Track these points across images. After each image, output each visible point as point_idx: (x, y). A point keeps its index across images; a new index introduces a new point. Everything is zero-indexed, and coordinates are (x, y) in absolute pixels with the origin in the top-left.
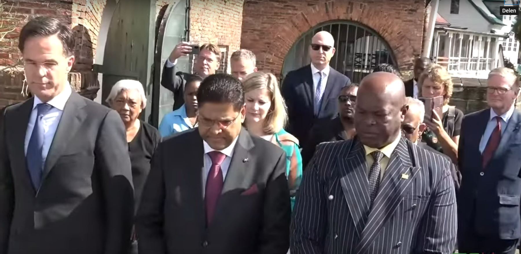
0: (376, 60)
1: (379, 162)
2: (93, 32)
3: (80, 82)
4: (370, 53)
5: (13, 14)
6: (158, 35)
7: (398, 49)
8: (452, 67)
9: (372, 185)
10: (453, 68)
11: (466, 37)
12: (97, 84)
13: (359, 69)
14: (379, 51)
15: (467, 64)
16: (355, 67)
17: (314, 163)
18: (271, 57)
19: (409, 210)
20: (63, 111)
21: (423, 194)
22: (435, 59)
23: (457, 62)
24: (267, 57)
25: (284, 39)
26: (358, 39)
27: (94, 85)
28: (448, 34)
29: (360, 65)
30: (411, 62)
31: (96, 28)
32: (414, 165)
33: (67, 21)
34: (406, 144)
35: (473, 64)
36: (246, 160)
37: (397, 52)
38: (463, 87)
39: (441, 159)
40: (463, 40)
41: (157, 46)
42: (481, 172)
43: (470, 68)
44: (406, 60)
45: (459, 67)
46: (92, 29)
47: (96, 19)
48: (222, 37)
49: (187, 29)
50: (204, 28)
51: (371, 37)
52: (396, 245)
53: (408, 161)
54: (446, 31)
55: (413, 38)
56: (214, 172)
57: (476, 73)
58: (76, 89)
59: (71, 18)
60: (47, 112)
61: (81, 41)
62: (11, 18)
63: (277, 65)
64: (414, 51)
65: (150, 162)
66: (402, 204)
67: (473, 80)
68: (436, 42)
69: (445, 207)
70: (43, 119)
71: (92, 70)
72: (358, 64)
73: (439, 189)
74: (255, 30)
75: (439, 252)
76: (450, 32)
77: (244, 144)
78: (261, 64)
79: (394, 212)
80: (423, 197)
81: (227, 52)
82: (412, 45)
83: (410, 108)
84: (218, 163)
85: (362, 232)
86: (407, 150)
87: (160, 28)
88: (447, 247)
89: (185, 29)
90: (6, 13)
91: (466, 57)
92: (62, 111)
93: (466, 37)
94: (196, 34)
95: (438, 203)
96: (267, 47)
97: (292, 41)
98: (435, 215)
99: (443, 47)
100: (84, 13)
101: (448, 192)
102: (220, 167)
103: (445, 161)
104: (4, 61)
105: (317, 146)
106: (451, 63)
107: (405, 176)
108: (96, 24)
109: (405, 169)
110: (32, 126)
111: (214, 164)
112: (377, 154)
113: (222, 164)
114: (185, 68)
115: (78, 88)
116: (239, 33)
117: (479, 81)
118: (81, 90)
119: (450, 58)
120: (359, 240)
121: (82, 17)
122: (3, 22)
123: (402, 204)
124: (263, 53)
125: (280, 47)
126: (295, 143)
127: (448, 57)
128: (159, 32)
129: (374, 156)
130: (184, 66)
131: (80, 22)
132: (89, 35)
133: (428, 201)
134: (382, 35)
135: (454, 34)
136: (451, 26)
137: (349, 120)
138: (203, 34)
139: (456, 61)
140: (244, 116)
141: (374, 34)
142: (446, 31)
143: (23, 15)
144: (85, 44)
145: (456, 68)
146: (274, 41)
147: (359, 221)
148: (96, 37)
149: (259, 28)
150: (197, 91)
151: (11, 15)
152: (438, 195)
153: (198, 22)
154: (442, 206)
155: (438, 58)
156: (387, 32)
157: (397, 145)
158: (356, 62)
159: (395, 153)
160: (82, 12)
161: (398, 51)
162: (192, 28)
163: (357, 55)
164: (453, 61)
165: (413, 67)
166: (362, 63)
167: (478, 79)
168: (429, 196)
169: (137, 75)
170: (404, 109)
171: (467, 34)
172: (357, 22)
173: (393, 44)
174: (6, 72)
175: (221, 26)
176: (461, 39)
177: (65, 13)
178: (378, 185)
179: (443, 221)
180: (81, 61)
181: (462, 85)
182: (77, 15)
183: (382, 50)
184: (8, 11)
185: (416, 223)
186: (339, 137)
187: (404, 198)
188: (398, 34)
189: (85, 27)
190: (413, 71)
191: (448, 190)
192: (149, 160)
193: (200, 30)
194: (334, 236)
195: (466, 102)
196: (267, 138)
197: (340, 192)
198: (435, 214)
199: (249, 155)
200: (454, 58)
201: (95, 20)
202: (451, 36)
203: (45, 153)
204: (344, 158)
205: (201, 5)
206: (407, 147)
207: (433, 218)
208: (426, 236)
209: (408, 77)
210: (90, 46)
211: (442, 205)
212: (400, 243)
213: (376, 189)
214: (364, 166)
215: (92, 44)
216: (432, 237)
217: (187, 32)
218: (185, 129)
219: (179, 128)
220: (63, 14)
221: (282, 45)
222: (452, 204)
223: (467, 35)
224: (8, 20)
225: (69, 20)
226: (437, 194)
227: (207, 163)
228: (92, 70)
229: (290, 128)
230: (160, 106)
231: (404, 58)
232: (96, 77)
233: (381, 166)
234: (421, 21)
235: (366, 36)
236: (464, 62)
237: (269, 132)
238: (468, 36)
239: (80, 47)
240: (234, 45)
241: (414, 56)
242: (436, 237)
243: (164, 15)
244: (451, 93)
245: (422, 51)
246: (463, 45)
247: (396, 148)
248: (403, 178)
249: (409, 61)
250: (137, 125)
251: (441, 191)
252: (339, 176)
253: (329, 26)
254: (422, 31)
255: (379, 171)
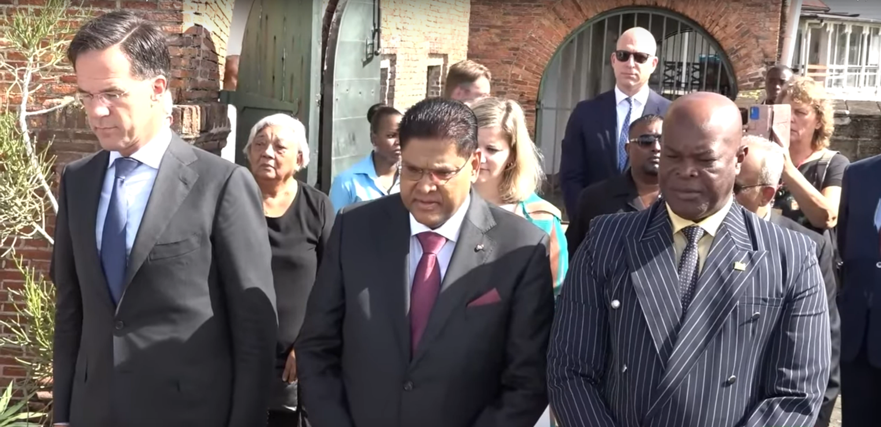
0: (700, 74)
1: (697, 243)
2: (219, 37)
3: (199, 120)
4: (689, 61)
5: (87, 9)
6: (329, 39)
7: (738, 54)
8: (833, 82)
9: (686, 283)
10: (835, 84)
11: (857, 31)
12: (227, 124)
13: (671, 89)
14: (704, 58)
15: (859, 76)
16: (664, 86)
17: (587, 247)
18: (520, 72)
19: (749, 322)
20: (158, 170)
21: (770, 295)
22: (803, 70)
23: (841, 74)
24: (513, 72)
25: (540, 41)
26: (669, 39)
27: (223, 125)
28: (826, 25)
29: (673, 81)
30: (761, 75)
31: (224, 28)
32: (755, 248)
33: (175, 19)
34: (741, 213)
35: (870, 76)
36: (479, 247)
37: (736, 58)
38: (850, 116)
39: (800, 238)
40: (852, 35)
41: (326, 57)
42: (878, 262)
43: (865, 83)
44: (751, 71)
45: (844, 83)
46: (218, 32)
47: (224, 15)
48: (436, 40)
49: (376, 28)
50: (405, 26)
51: (691, 33)
52: (726, 380)
53: (745, 241)
54: (822, 20)
55: (762, 34)
56: (426, 267)
57: (876, 92)
58: (192, 132)
59: (182, 14)
60: (131, 172)
61: (200, 53)
62: (83, 16)
63: (530, 84)
64: (766, 56)
65: (317, 250)
66: (735, 311)
67: (869, 103)
68: (805, 40)
69: (809, 317)
70: (124, 185)
71: (219, 100)
72: (669, 81)
73: (798, 287)
74: (491, 27)
75: (802, 392)
76: (828, 23)
77: (477, 221)
78: (504, 85)
79: (722, 325)
80: (771, 301)
81: (445, 65)
82: (762, 46)
83: (749, 151)
84: (433, 252)
85: (668, 359)
86: (744, 224)
87: (331, 28)
88: (814, 384)
89: (373, 29)
90: (76, 8)
91: (857, 64)
92: (156, 169)
93: (857, 31)
94: (392, 36)
95: (797, 310)
96: (512, 55)
97: (555, 44)
98: (793, 330)
99: (816, 48)
100: (204, 5)
101: (814, 292)
102: (436, 259)
103: (808, 242)
104: (73, 88)
105: (592, 220)
106: (832, 75)
107: (740, 266)
108: (224, 23)
109: (739, 253)
110: (107, 196)
111: (426, 254)
112: (693, 231)
113: (441, 253)
114: (373, 95)
115: (196, 131)
116: (464, 31)
117: (878, 106)
118: (200, 134)
119: (829, 66)
120: (663, 373)
121: (199, 12)
122: (70, 24)
123: (735, 311)
124: (508, 65)
125: (535, 54)
126: (554, 216)
127: (825, 65)
128: (330, 33)
129: (688, 233)
130: (372, 91)
131: (197, 20)
132: (212, 42)
133: (779, 308)
134: (709, 31)
135: (835, 26)
136: (830, 12)
137: (651, 176)
138: (404, 35)
139: (840, 71)
140: (477, 171)
141: (695, 28)
142: (822, 21)
143: (103, 10)
144: (206, 57)
145: (839, 83)
146: (525, 45)
147: (791, 412)
148: (223, 45)
149: (499, 23)
150: (398, 130)
151: (83, 12)
152: (798, 297)
153: (395, 16)
154: (805, 316)
155: (808, 66)
156: (717, 25)
157: (727, 216)
158: (666, 78)
159: (722, 229)
160: (200, 3)
161: (737, 56)
162: (385, 26)
163: (668, 65)
164: (834, 71)
165: (763, 84)
166: (677, 78)
167: (877, 102)
168: (782, 299)
169: (290, 106)
170: (741, 154)
171: (858, 24)
172: (665, 9)
173: (728, 45)
174: (77, 107)
175: (435, 20)
176: (847, 33)
177: (172, 5)
178: (696, 283)
179: (806, 342)
180: (198, 86)
181: (847, 112)
182: (192, 8)
183: (710, 56)
184: (78, 5)
185: (760, 346)
186: (629, 206)
187: (738, 302)
188: (737, 28)
189: (205, 29)
190: (764, 90)
191: (813, 289)
192: (314, 246)
193: (398, 29)
194: (621, 367)
195: (856, 142)
196: (508, 208)
197: (629, 294)
198: (792, 330)
199: (485, 239)
200: (835, 67)
201: (221, 16)
202: (830, 29)
203: (130, 242)
204: (637, 239)
205: (392, 6)
206: (742, 218)
207: (790, 336)
208: (778, 368)
209: (754, 101)
210: (215, 60)
211: (804, 313)
212: (733, 378)
213: (691, 288)
214: (672, 251)
215: (217, 58)
216: (789, 367)
217: (377, 34)
218: (376, 196)
219: (367, 194)
220: (169, 7)
221: (537, 51)
222: (821, 313)
223: (858, 27)
224: (79, 20)
225: (178, 17)
226: (796, 295)
227: (415, 254)
228: (219, 100)
229: (547, 191)
230: (333, 158)
231: (748, 69)
232: (224, 111)
233: (700, 251)
234: (776, 4)
235: (683, 31)
236: (854, 74)
237: (510, 200)
238: (861, 29)
239: (198, 62)
240: (457, 53)
241: (765, 65)
242: (795, 368)
243: (338, 6)
244: (833, 129)
245: (780, 56)
246: (853, 43)
247: (725, 220)
248: (736, 270)
249: (757, 74)
250: (288, 191)
251: (802, 290)
252: (628, 269)
253: (619, 16)
254: (777, 22)
255: (697, 258)
